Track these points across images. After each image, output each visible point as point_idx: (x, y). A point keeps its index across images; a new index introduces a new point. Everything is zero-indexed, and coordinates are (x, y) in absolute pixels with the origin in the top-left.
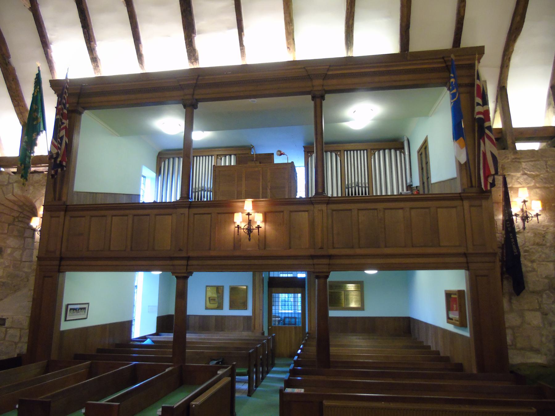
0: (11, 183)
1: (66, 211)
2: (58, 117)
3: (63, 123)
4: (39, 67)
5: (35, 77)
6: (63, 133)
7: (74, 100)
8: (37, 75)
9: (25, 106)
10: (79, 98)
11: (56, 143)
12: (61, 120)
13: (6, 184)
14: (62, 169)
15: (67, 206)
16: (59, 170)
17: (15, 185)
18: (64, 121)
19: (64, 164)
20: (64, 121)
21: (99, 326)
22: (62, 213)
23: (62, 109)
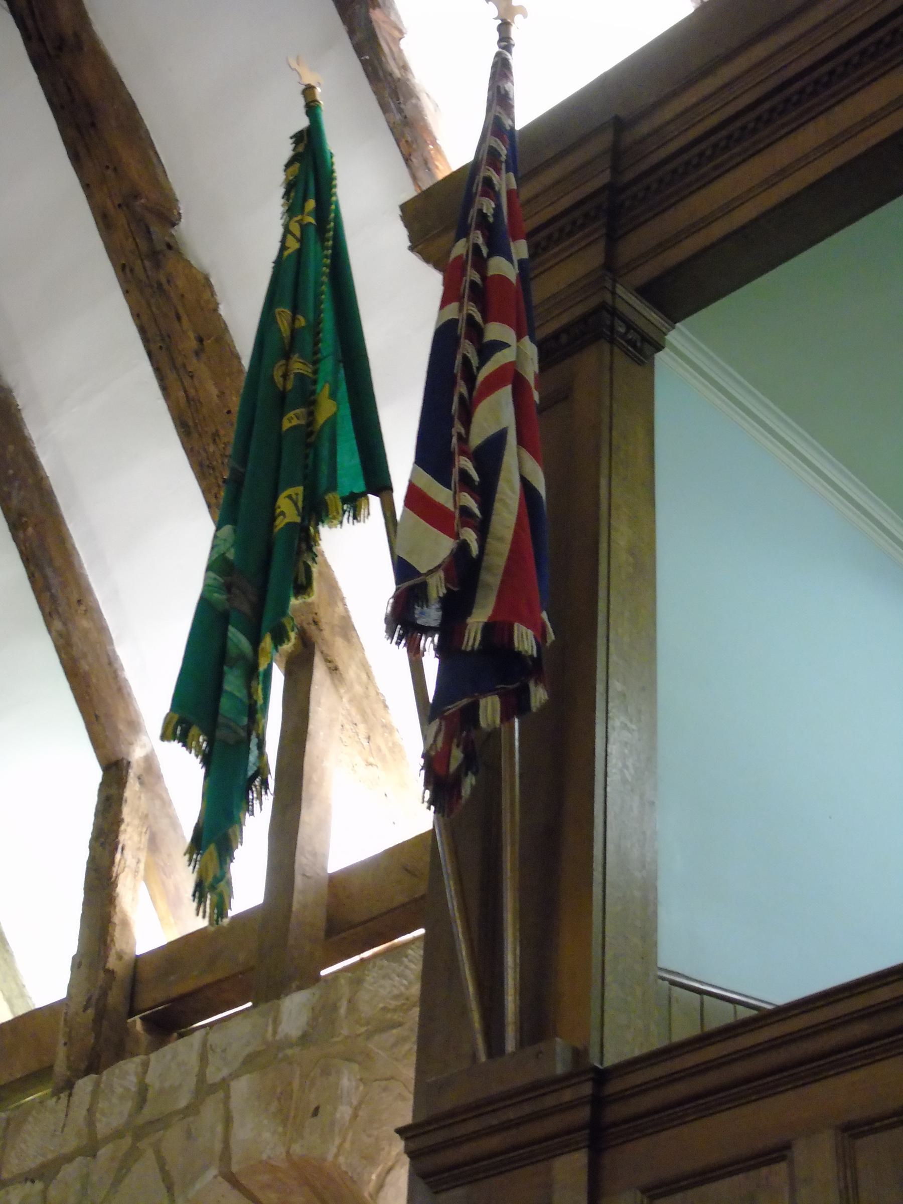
0: (213, 1088)
1: (598, 1138)
2: (452, 311)
3: (487, 350)
4: (308, 91)
5: (287, 151)
6: (496, 414)
7: (578, 265)
8: (298, 138)
9: (214, 335)
10: (612, 239)
11: (442, 495)
12: (475, 331)
13: (183, 1103)
14: (517, 704)
15: (601, 1076)
16: (490, 709)
17: (241, 1087)
18: (495, 331)
19: (525, 640)
20: (495, 331)
21: (408, 202)
22: (570, 1168)
23: (480, 263)
